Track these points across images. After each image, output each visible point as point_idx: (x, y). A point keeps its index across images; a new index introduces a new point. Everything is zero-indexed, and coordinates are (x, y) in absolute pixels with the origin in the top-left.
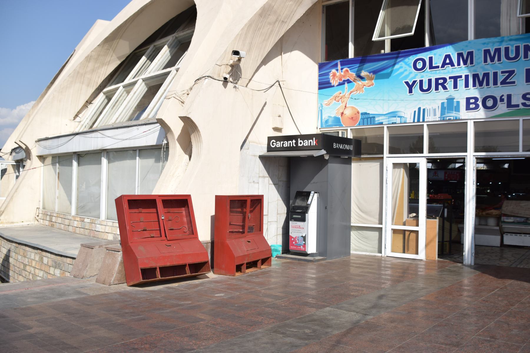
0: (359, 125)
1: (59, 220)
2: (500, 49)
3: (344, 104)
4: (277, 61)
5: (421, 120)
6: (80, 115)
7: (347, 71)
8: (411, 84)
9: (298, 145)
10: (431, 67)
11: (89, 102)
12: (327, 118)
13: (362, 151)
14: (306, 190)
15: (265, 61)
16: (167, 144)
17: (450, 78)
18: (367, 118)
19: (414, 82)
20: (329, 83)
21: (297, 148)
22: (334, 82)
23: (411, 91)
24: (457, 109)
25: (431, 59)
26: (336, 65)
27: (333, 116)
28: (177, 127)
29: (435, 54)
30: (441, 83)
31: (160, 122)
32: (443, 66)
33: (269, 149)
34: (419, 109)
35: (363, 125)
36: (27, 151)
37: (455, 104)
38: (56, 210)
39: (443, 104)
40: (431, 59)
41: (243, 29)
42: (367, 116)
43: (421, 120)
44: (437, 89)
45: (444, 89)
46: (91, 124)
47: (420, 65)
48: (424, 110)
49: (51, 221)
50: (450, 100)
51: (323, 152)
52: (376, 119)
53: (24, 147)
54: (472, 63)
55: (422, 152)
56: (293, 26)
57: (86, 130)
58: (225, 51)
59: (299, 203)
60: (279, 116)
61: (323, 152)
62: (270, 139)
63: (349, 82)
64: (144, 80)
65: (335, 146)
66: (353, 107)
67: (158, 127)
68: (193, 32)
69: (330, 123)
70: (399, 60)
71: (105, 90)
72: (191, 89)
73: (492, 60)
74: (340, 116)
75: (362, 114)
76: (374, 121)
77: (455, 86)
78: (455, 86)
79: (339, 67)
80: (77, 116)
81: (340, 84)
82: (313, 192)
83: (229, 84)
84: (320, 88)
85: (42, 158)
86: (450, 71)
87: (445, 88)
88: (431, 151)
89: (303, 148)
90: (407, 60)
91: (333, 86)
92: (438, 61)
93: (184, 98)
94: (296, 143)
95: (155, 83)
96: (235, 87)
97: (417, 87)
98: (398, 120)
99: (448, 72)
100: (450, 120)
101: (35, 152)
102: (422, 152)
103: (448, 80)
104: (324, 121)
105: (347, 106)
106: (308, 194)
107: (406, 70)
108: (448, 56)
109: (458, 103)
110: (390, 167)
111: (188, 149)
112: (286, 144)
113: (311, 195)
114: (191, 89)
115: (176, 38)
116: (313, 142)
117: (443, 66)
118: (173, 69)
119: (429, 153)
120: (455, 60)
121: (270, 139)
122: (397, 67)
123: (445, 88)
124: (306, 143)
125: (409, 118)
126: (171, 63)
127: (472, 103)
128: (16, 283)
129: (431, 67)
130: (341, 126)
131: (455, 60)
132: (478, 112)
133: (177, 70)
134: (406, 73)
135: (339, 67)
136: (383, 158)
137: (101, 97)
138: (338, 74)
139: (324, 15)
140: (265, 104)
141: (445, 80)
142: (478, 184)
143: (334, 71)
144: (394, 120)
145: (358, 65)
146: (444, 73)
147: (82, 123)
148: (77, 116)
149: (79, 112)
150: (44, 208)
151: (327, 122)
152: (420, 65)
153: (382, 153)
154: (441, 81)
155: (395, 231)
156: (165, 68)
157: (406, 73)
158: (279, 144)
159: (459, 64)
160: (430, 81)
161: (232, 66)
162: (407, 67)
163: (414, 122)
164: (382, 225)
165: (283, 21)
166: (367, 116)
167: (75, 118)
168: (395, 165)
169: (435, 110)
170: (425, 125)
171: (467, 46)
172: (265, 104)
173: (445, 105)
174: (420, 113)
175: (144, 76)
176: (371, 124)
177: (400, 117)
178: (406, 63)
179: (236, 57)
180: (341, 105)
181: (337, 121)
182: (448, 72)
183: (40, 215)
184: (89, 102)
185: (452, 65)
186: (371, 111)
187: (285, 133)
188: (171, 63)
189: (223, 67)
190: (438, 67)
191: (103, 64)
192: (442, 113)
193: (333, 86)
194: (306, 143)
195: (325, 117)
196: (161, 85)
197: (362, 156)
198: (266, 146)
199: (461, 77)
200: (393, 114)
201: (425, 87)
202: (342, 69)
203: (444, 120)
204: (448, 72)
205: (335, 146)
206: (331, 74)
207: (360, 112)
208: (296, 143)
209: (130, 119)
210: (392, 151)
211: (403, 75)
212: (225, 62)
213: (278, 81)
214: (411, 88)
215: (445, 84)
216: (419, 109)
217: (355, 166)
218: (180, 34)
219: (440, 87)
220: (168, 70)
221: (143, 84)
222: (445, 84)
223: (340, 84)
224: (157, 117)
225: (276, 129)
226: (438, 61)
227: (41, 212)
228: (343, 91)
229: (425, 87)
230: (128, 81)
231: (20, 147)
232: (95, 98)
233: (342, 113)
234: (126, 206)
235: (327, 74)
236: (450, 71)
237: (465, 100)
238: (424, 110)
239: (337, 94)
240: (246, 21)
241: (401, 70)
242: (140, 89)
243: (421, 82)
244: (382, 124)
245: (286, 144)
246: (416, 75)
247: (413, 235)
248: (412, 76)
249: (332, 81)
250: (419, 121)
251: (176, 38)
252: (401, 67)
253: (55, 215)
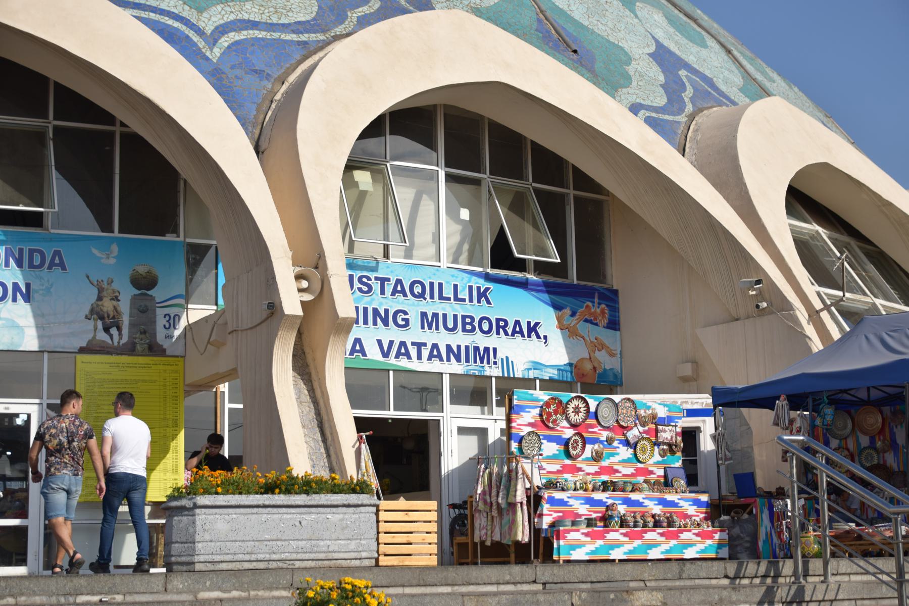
2: (438, 314)
9: (356, 347)
45: (488, 304)
48: (440, 285)
73: (430, 328)
86: (400, 302)
127: (468, 324)
128: (607, 303)
132: (490, 338)
135: (596, 300)
142: (107, 148)
163: (748, 562)
164: (735, 475)
202: (600, 304)
215: (507, 329)
219: (501, 330)
222: (507, 329)
236: (400, 302)
238: (440, 285)
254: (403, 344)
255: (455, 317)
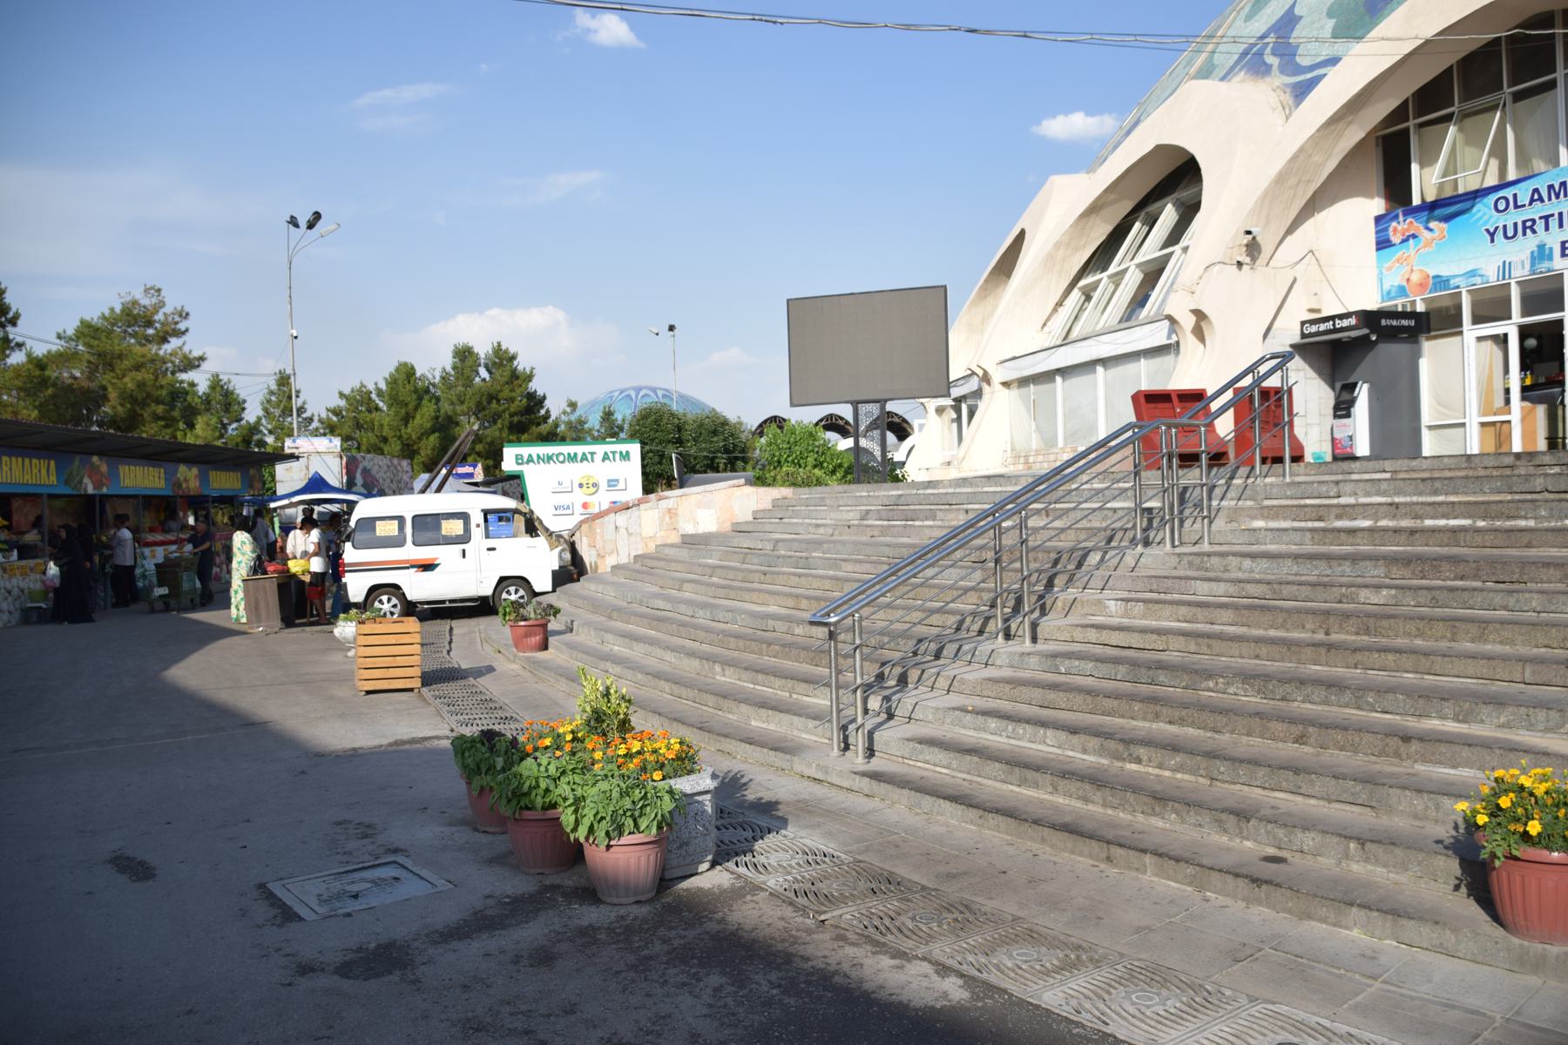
0: (1430, 292)
1: (1040, 458)
3: (1409, 267)
4: (1308, 226)
5: (1507, 276)
6: (1049, 324)
7: (1411, 223)
8: (1492, 231)
10: (1516, 207)
11: (1060, 304)
12: (1389, 288)
13: (1433, 325)
14: (1351, 380)
15: (1290, 230)
16: (1178, 343)
17: (1541, 218)
18: (1440, 282)
19: (1497, 228)
20: (1388, 241)
21: (1335, 330)
22: (1396, 239)
23: (1492, 241)
24: (1550, 258)
25: (1515, 196)
26: (1396, 217)
27: (1396, 284)
28: (1188, 322)
29: (1520, 190)
30: (1529, 227)
31: (1170, 318)
32: (1530, 204)
33: (1303, 336)
34: (1504, 262)
35: (1436, 291)
36: (986, 378)
37: (1547, 252)
38: (1034, 447)
39: (1532, 253)
40: (1515, 196)
41: (1256, 202)
42: (1439, 279)
43: (1507, 276)
44: (1524, 234)
46: (1064, 334)
47: (1502, 205)
49: (1027, 463)
50: (1541, 247)
51: (1365, 331)
52: (1452, 282)
53: (980, 373)
54: (1565, 196)
55: (1510, 318)
56: (1331, 176)
57: (1059, 342)
58: (1236, 232)
59: (1345, 396)
60: (1316, 294)
61: (1365, 331)
62: (1303, 323)
63: (1414, 236)
64: (1138, 266)
65: (1383, 322)
66: (1421, 271)
67: (1166, 323)
68: (1201, 190)
69: (1393, 294)
70: (1477, 200)
71: (1082, 283)
72: (1200, 278)
73: (1557, 196)
74: (1405, 284)
75: (1434, 277)
76: (1449, 285)
77: (1547, 228)
78: (1547, 228)
79: (1401, 218)
80: (1045, 325)
81: (1403, 241)
82: (1360, 383)
83: (1245, 267)
84: (1378, 249)
85: (1006, 384)
87: (1534, 232)
88: (1525, 313)
89: (1342, 330)
90: (1485, 200)
91: (1394, 245)
92: (1524, 199)
93: (1193, 289)
94: (1334, 325)
95: (1154, 267)
96: (1252, 268)
97: (1500, 232)
98: (1478, 280)
99: (1537, 211)
100: (1541, 272)
101: (998, 376)
102: (1510, 318)
103: (1538, 221)
104: (1385, 292)
105: (1414, 268)
106: (1355, 385)
107: (1485, 214)
108: (1536, 190)
109: (1551, 249)
110: (1473, 341)
111: (1201, 338)
112: (1323, 327)
113: (1359, 385)
114: (1200, 278)
115: (1178, 200)
116: (1353, 321)
117: (1530, 204)
118: (1177, 249)
119: (1523, 316)
120: (1545, 195)
121: (1303, 323)
122: (1475, 210)
123: (1534, 232)
124: (1345, 323)
125: (1492, 277)
126: (1175, 237)
129: (1516, 207)
130: (1407, 296)
131: (1545, 195)
133: (1185, 249)
134: (1487, 217)
135: (1401, 218)
136: (1461, 333)
137: (1076, 295)
138: (1400, 228)
139: (1380, 150)
140: (1295, 280)
141: (1534, 221)
143: (1394, 224)
144: (1473, 280)
145: (1426, 213)
146: (1533, 213)
147: (1052, 334)
148: (1045, 325)
149: (1048, 320)
150: (1012, 450)
151: (1389, 293)
152: (1502, 205)
153: (1460, 324)
154: (1529, 224)
155: (1483, 425)
156: (1163, 247)
157: (1487, 217)
158: (1314, 329)
159: (1550, 199)
160: (1515, 225)
161: (1247, 246)
162: (1487, 211)
165: (1308, 181)
166: (1439, 279)
167: (1042, 328)
168: (1480, 339)
169: (1523, 262)
170: (1513, 282)
171: (1558, 175)
172: (1295, 280)
173: (1536, 254)
174: (1506, 268)
175: (1137, 261)
176: (1445, 290)
177: (1482, 276)
178: (1485, 205)
179: (1250, 237)
180: (1405, 270)
181: (1402, 291)
182: (1537, 211)
183: (1009, 460)
184: (1060, 304)
185: (1541, 199)
186: (1445, 273)
187: (1325, 314)
188: (1175, 237)
189: (1236, 249)
190: (1524, 206)
191: (1076, 249)
192: (1533, 264)
193: (1394, 245)
194: (1345, 323)
195: (1386, 287)
196: (1164, 268)
197: (1433, 334)
198: (1299, 332)
199: (1553, 215)
200: (1472, 273)
201: (1510, 233)
202: (1405, 221)
203: (1534, 274)
204: (1538, 211)
205: (1383, 322)
206: (1391, 229)
207: (1431, 275)
208: (1334, 325)
209: (1120, 322)
210: (1478, 319)
211: (1482, 221)
212: (1238, 243)
213: (1311, 251)
214: (1492, 235)
216: (1504, 262)
217: (1428, 346)
218: (1185, 194)
219: (1528, 231)
220: (1170, 250)
221: (1137, 270)
223: (1403, 241)
224: (1165, 313)
225: (1311, 311)
226: (1524, 199)
227: (1009, 456)
228: (1408, 249)
229: (1510, 233)
230: (1113, 269)
231: (974, 373)
232: (1066, 297)
233: (1408, 280)
234: (1142, 400)
235: (1386, 229)
237: (1559, 245)
239: (1399, 254)
240: (1259, 193)
241: (1479, 215)
242: (1133, 278)
243: (1505, 227)
244: (1458, 287)
245: (1323, 327)
246: (1498, 219)
247: (1505, 426)
248: (1492, 220)
249: (1392, 238)
250: (1504, 279)
251: (1178, 200)
252: (1479, 211)
253: (1032, 453)
254: (584, 454)
255: (1515, 225)
